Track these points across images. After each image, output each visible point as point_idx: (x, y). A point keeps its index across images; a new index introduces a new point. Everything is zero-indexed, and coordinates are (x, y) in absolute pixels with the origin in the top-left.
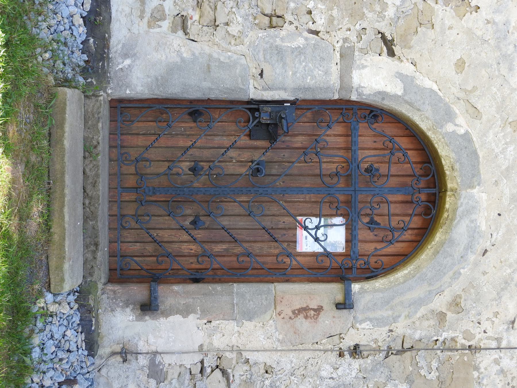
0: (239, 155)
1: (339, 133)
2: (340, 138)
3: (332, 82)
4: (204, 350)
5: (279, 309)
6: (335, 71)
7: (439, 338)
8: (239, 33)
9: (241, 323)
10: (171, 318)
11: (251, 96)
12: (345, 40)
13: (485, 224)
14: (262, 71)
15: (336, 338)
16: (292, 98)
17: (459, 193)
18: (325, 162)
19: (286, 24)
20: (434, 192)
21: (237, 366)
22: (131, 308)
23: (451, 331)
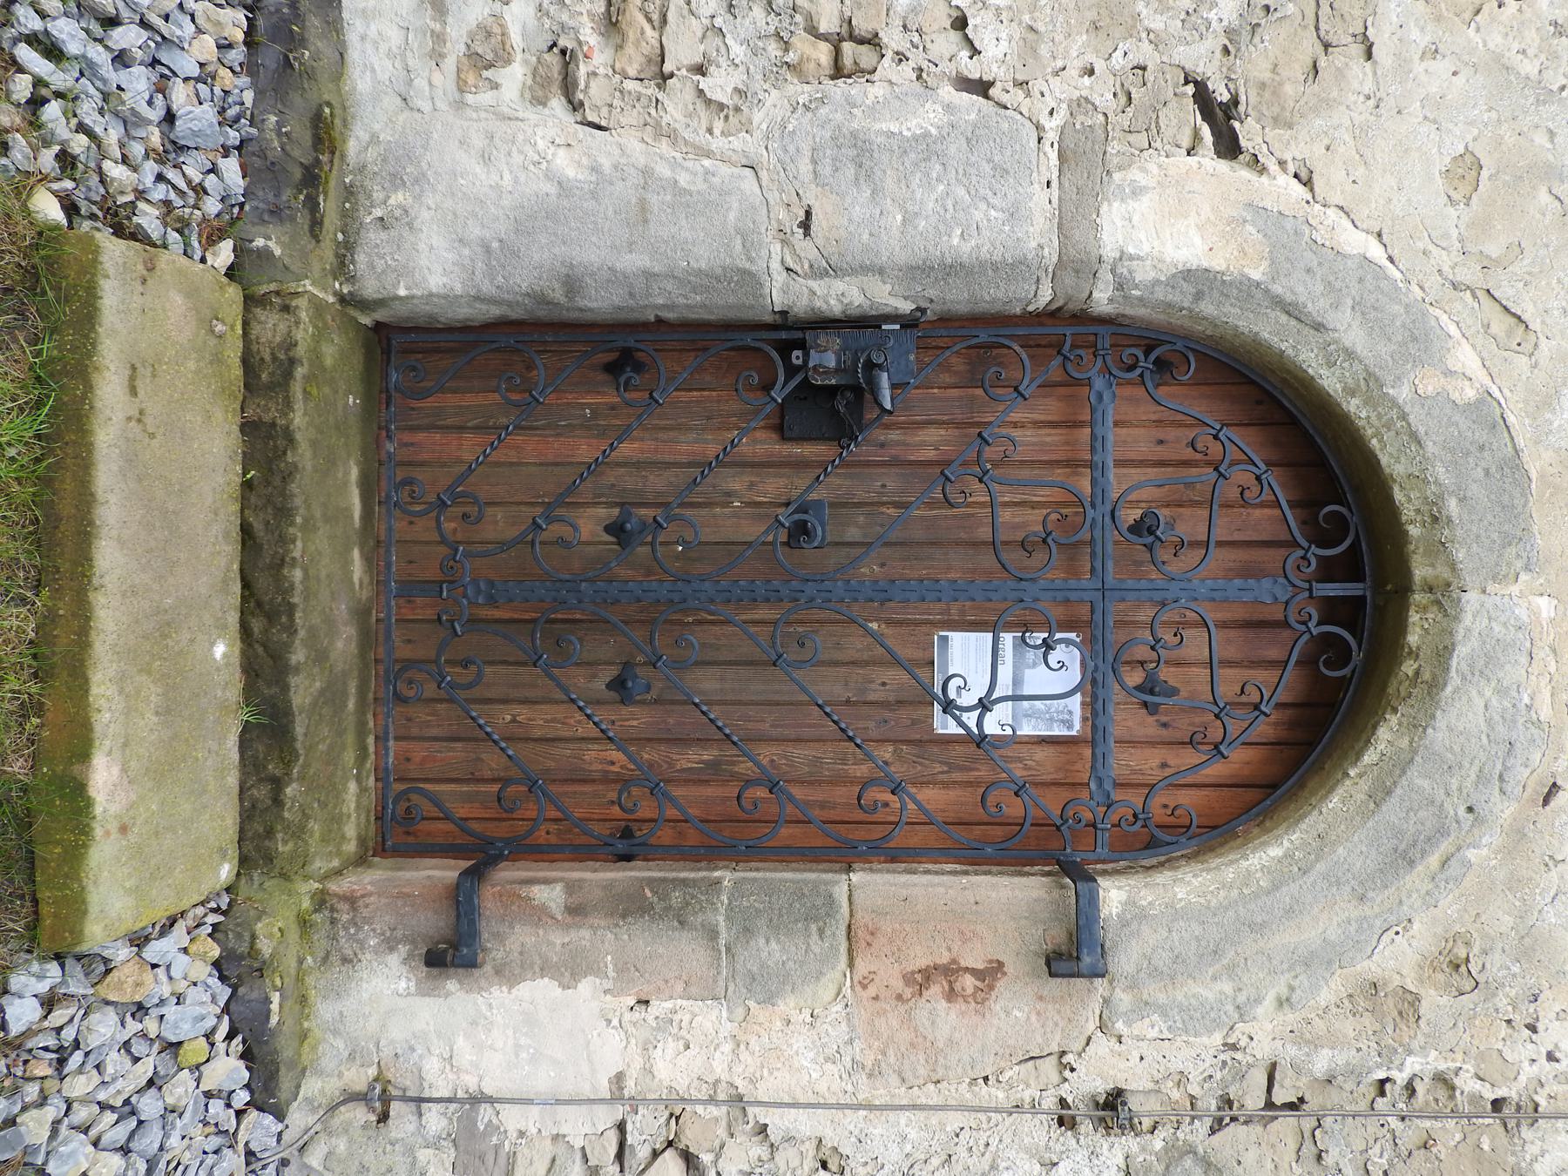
0: (752, 484)
1: (1050, 418)
2: (1053, 431)
3: (1033, 244)
4: (626, 1093)
5: (862, 966)
6: (1041, 204)
7: (1394, 1074)
8: (736, 98)
9: (740, 1011)
10: (525, 989)
11: (779, 300)
12: (1082, 104)
13: (1548, 700)
14: (808, 214)
15: (1049, 1066)
16: (906, 307)
17: (1459, 600)
18: (1005, 504)
19: (886, 61)
20: (1360, 593)
21: (730, 1142)
22: (404, 955)
23: (1434, 1054)
